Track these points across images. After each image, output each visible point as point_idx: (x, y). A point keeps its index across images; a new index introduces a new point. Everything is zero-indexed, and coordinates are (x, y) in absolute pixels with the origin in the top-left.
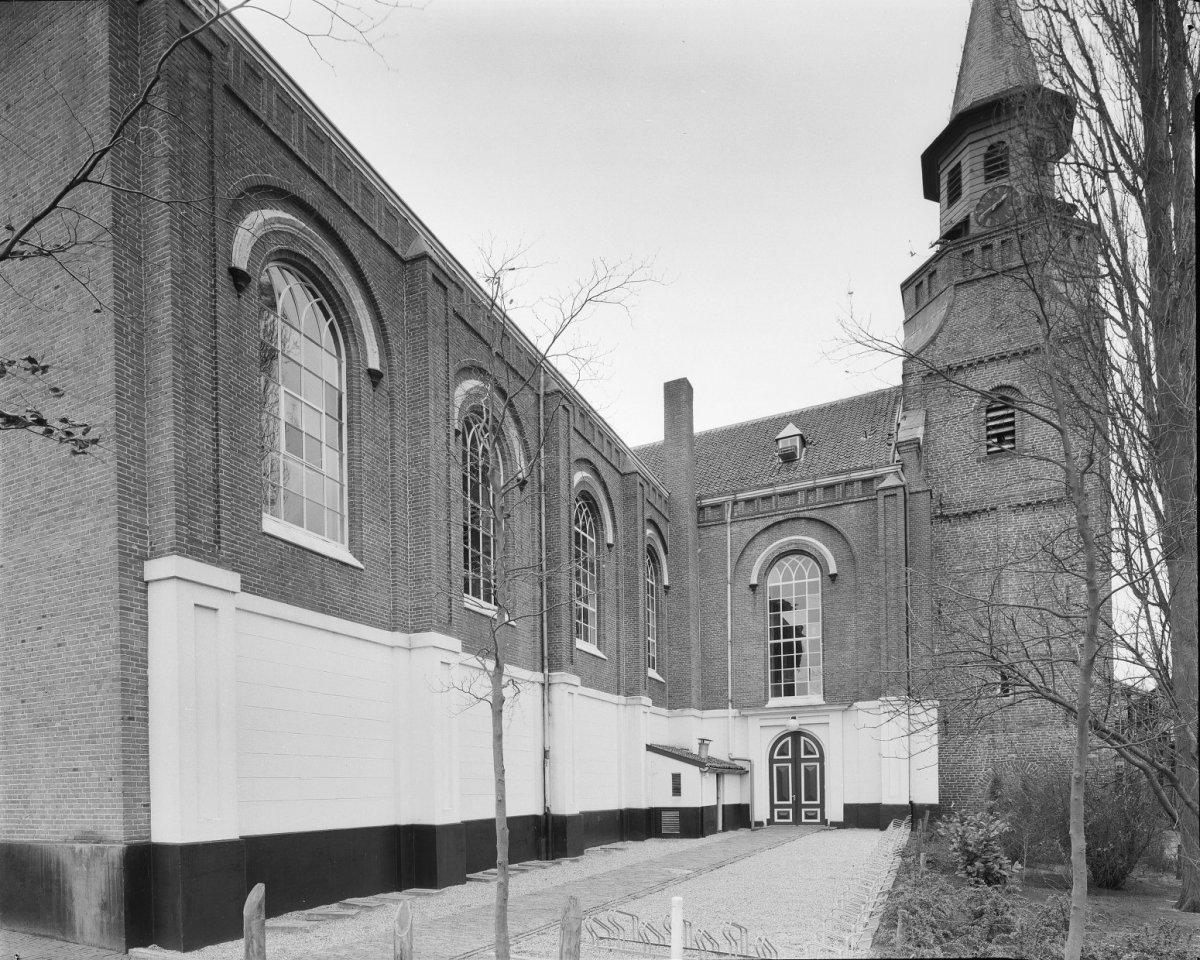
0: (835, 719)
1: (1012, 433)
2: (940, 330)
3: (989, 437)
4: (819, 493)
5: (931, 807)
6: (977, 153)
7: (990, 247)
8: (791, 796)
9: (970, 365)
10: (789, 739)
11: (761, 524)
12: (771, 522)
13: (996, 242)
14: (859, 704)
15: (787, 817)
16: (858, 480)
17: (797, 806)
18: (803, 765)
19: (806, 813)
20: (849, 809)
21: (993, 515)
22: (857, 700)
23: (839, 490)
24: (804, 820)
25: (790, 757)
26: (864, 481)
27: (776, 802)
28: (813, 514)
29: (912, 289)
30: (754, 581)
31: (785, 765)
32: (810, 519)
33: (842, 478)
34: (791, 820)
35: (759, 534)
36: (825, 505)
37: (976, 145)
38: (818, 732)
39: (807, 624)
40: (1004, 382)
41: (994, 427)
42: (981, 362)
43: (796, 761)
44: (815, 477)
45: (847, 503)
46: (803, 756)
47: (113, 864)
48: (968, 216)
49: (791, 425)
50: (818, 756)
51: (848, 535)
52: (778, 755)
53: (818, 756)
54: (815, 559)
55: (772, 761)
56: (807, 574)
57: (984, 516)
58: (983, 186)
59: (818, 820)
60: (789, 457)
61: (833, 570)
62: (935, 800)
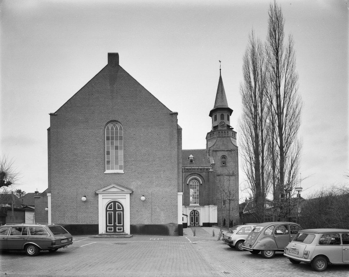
0: (202, 208)
1: (225, 163)
2: (215, 144)
3: (222, 163)
5: (216, 223)
10: (113, 203)
11: (189, 173)
13: (223, 132)
14: (205, 206)
15: (193, 225)
17: (195, 223)
18: (117, 212)
19: (109, 228)
23: (202, 170)
24: (117, 231)
26: (207, 169)
27: (108, 225)
28: (198, 173)
29: (209, 134)
30: (188, 183)
34: (113, 231)
37: (219, 113)
38: (199, 211)
41: (223, 161)
43: (194, 215)
44: (199, 167)
50: (122, 209)
52: (109, 209)
53: (122, 209)
54: (198, 181)
55: (107, 211)
60: (191, 161)
61: (201, 183)
62: (217, 222)
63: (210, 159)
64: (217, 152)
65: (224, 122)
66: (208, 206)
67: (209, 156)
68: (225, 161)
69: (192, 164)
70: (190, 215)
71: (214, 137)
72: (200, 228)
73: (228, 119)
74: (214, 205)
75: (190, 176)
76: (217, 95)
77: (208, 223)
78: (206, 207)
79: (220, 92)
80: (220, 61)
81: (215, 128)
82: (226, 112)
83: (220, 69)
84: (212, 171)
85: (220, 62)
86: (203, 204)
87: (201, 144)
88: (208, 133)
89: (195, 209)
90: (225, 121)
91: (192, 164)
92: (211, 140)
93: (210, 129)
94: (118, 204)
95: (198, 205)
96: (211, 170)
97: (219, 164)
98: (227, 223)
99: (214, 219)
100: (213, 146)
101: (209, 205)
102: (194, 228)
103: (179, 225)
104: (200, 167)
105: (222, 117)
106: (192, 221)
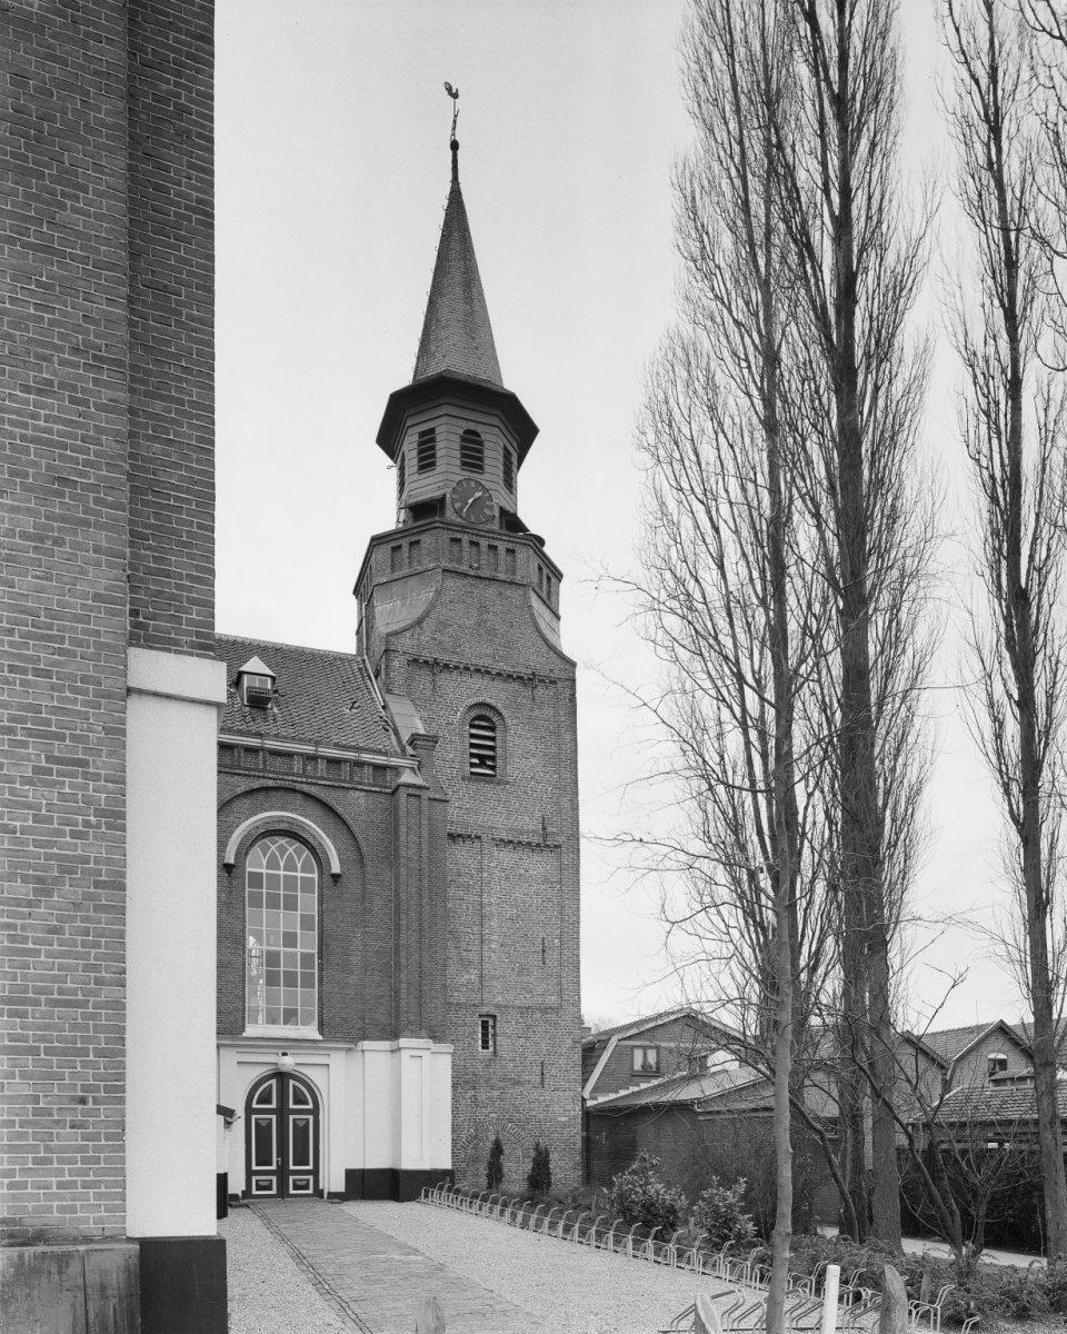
0: (337, 1060)
1: (493, 758)
2: (427, 614)
3: (472, 755)
4: (322, 765)
5: (445, 1173)
6: (454, 429)
7: (458, 541)
8: (274, 1159)
9: (456, 668)
12: (256, 784)
14: (366, 1044)
15: (269, 1188)
16: (369, 764)
17: (283, 1173)
18: (291, 1117)
20: (351, 1175)
21: (477, 844)
22: (364, 1039)
23: (346, 768)
24: (292, 1192)
25: (274, 1106)
26: (377, 768)
27: (254, 1168)
28: (313, 790)
30: (232, 861)
31: (305, 1117)
32: (307, 795)
33: (350, 755)
34: (274, 1192)
35: (238, 797)
36: (328, 783)
38: (315, 1076)
39: (299, 931)
40: (488, 701)
42: (467, 669)
43: (282, 1112)
44: (317, 744)
45: (357, 789)
46: (292, 1106)
47: (103, 1288)
48: (444, 495)
49: (256, 658)
50: (310, 1106)
51: (355, 829)
53: (310, 1106)
54: (312, 850)
56: (282, 865)
57: (468, 842)
58: (458, 470)
59: (310, 1191)
61: (336, 868)
63: (392, 706)
64: (444, 679)
65: (486, 490)
66: (386, 1045)
67: (389, 691)
68: (492, 748)
69: (265, 720)
70: (249, 1111)
71: (420, 568)
72: (322, 1208)
73: (510, 483)
74: (434, 1038)
75: (247, 801)
76: (432, 303)
77: (359, 1170)
78: (375, 1051)
79: (456, 276)
80: (449, 89)
81: (422, 512)
82: (495, 421)
83: (455, 146)
84: (420, 787)
85: (455, 96)
86: (347, 1025)
87: (328, 624)
88: (377, 541)
89: (288, 1063)
90: (487, 485)
91: (265, 720)
92: (396, 587)
93: (388, 518)
94: (290, 854)
95: (311, 1032)
96: (407, 777)
97: (454, 754)
98: (517, 1171)
99: (429, 1150)
100: (411, 627)
101: (394, 1035)
102: (278, 1210)
103: (149, 1247)
104: (327, 745)
105: (472, 456)
106: (264, 1159)
